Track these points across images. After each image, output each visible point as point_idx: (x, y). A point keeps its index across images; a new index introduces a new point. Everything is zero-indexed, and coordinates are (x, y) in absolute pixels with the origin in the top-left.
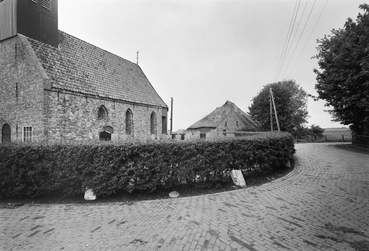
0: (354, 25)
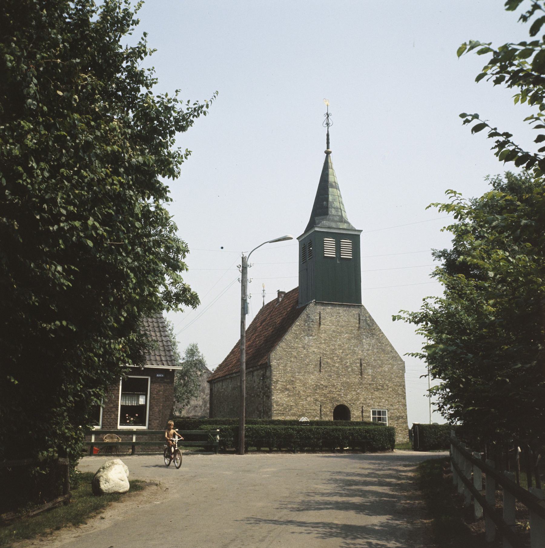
0: (149, 309)
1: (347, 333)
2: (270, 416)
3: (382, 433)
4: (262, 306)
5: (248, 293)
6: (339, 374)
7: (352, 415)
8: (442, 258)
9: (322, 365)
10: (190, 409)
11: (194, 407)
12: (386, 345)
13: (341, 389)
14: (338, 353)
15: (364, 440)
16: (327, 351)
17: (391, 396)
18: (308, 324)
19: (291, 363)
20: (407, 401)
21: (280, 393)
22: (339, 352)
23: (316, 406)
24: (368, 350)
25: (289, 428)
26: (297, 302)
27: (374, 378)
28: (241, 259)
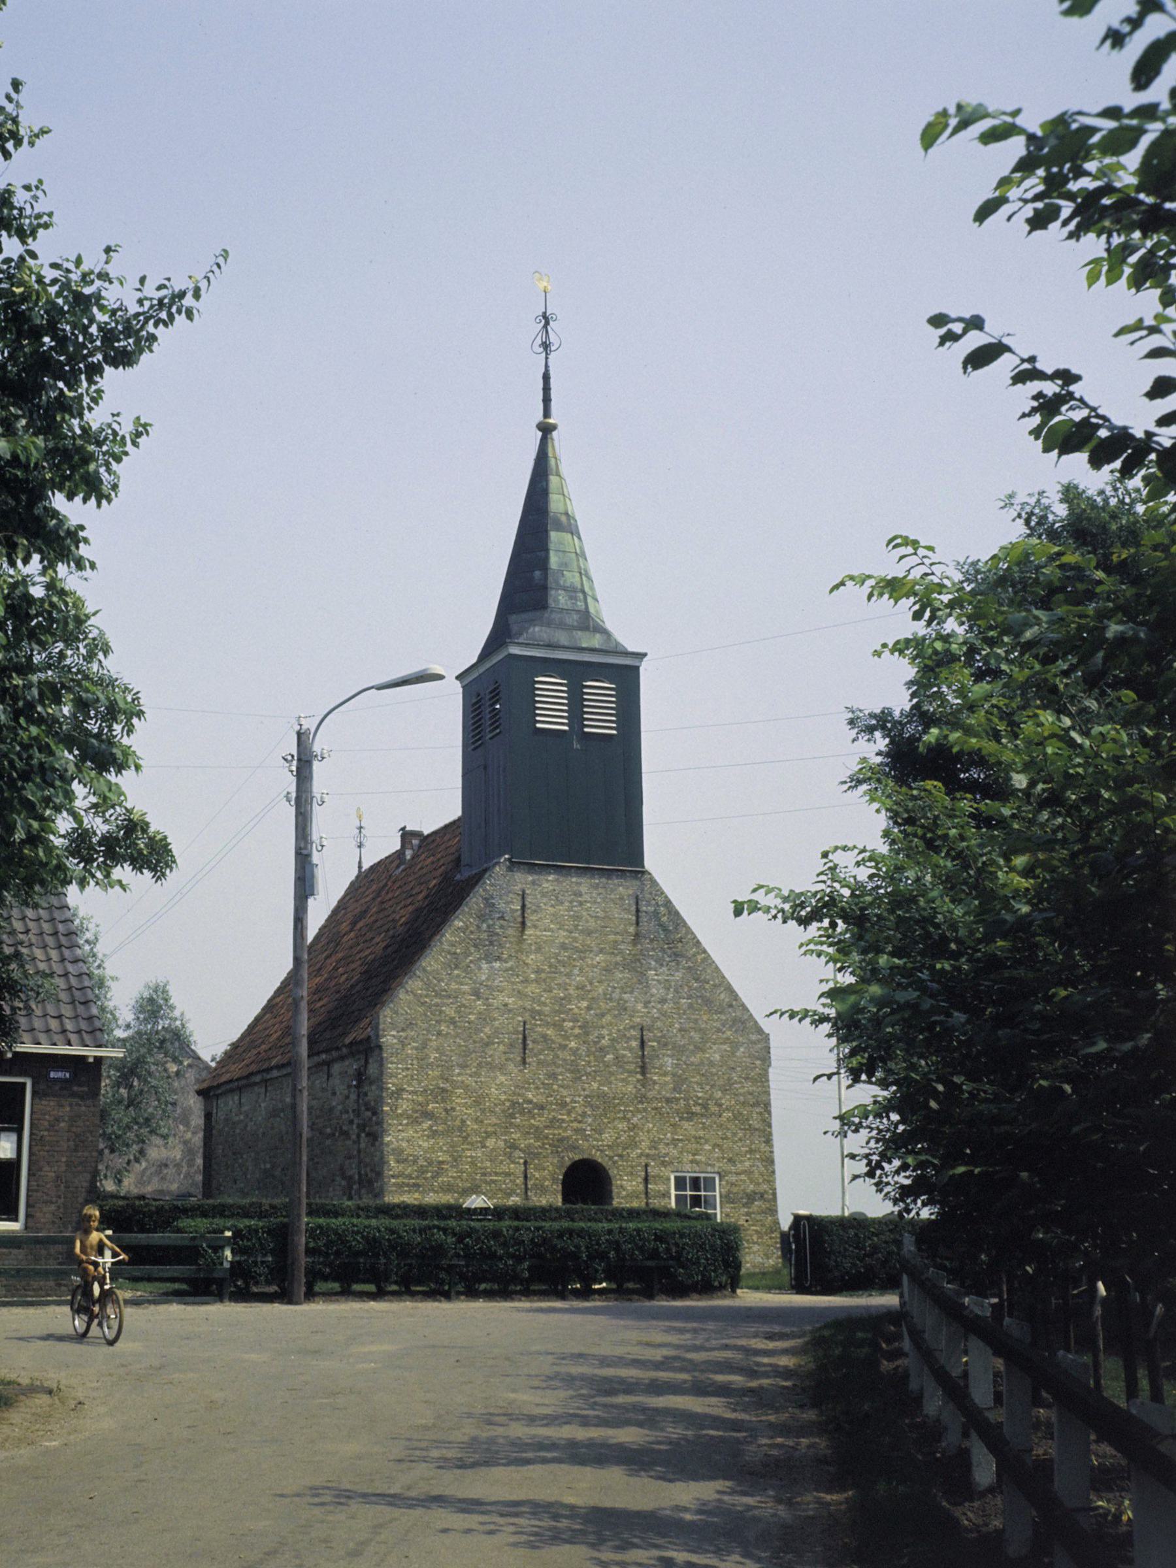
1: (601, 951)
2: (379, 1194)
3: (704, 1243)
4: (355, 872)
5: (315, 837)
6: (578, 1071)
7: (615, 1190)
8: (878, 734)
9: (530, 1045)
10: (148, 1173)
11: (160, 1166)
12: (715, 986)
13: (584, 1114)
14: (576, 1011)
15: (650, 1263)
16: (544, 1004)
17: (729, 1134)
18: (489, 927)
19: (441, 1039)
20: (775, 1149)
21: (407, 1125)
22: (579, 1008)
23: (513, 1162)
24: (663, 1001)
25: (435, 1227)
26: (458, 861)
27: (679, 1082)
28: (295, 737)
